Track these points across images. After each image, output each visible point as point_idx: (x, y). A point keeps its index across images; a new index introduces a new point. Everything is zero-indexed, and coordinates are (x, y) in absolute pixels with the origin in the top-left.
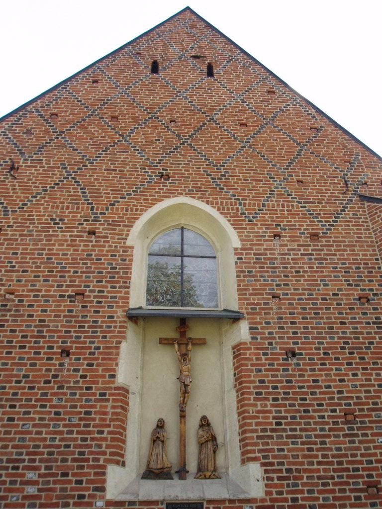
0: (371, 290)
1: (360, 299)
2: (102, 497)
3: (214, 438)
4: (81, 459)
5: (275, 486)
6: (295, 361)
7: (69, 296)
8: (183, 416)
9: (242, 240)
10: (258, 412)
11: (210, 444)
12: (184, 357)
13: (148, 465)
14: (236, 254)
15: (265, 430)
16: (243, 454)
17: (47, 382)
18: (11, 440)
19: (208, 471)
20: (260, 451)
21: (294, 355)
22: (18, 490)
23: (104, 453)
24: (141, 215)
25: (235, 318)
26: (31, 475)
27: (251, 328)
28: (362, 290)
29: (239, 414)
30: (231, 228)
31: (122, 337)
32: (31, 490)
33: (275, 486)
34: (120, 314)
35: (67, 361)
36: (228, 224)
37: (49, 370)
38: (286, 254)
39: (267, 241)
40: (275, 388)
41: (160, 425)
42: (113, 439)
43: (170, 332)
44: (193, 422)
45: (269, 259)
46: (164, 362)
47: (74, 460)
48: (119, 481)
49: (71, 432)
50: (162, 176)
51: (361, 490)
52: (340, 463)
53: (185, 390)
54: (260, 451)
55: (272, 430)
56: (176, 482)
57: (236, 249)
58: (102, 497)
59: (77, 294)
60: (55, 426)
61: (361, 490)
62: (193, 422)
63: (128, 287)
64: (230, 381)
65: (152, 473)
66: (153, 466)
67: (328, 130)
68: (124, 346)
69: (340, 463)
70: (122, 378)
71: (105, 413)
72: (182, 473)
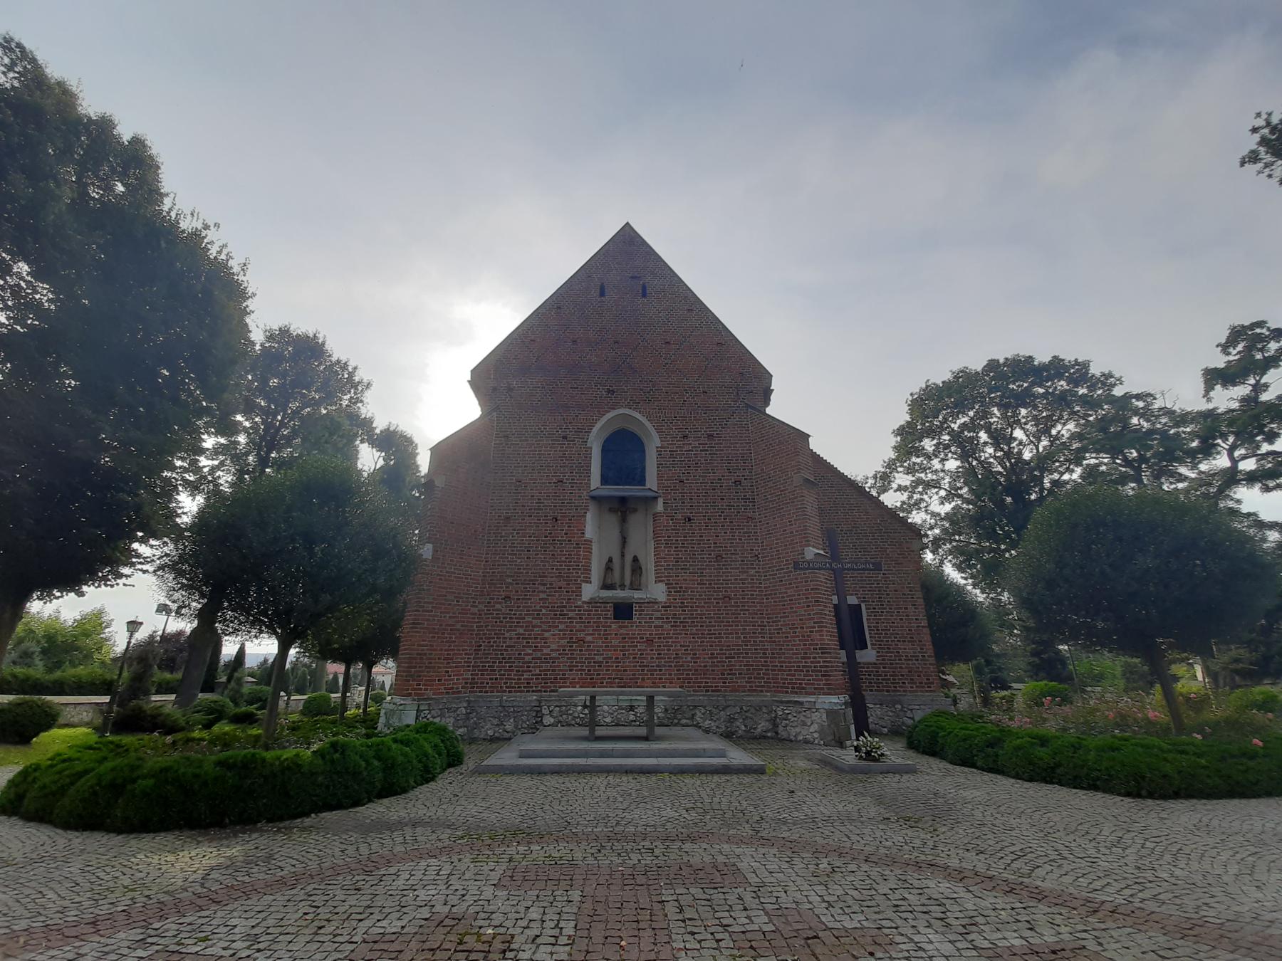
8: (623, 555)
12: (623, 520)
19: (635, 586)
41: (610, 560)
44: (629, 559)
50: (609, 391)
62: (629, 559)
65: (606, 586)
67: (238, 443)
68: (589, 515)
70: (588, 535)
72: (623, 587)
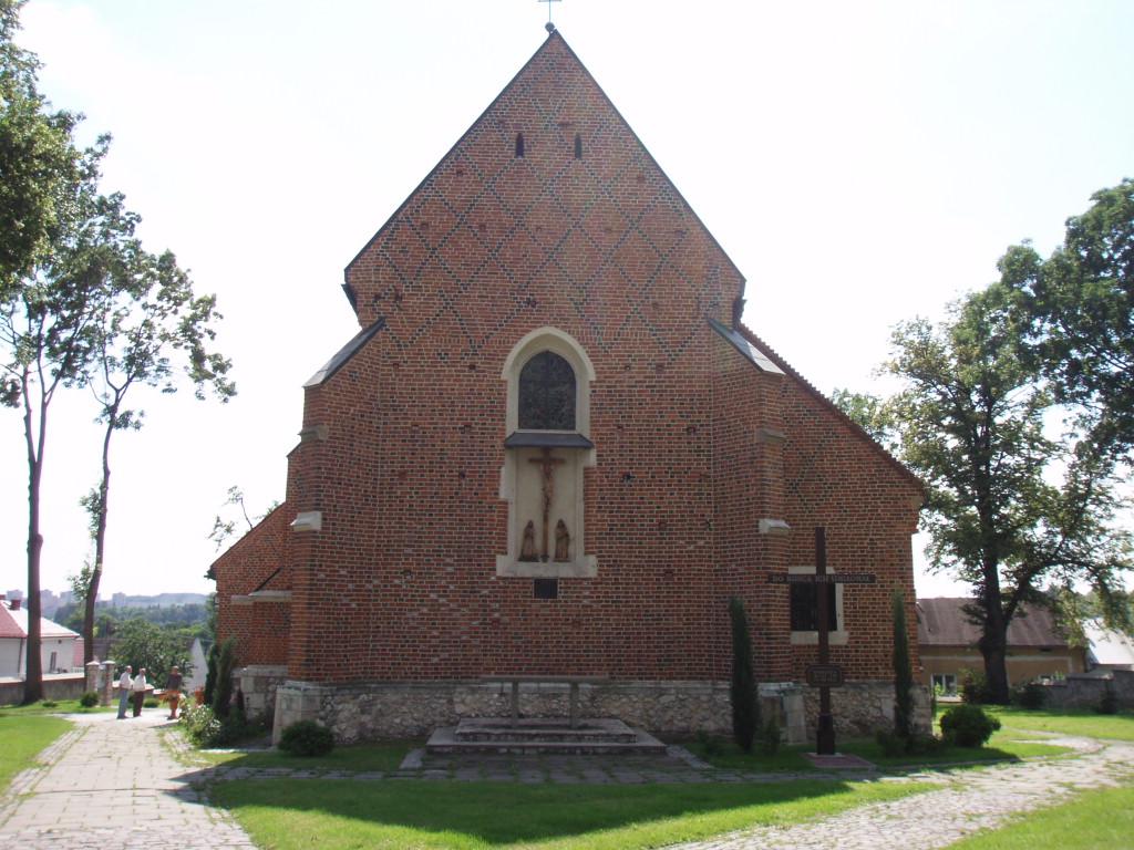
0: (699, 421)
1: (687, 430)
2: (494, 575)
3: (567, 535)
4: (479, 551)
5: (604, 570)
6: (629, 482)
7: (460, 428)
8: (546, 519)
9: (597, 373)
10: (598, 521)
11: (564, 540)
12: (547, 476)
13: (522, 551)
14: (592, 387)
15: (601, 534)
16: (586, 548)
17: (452, 498)
18: (434, 537)
19: (562, 557)
20: (596, 548)
21: (629, 477)
22: (443, 569)
23: (494, 547)
24: (511, 347)
25: (588, 447)
26: (448, 560)
27: (598, 456)
28: (692, 421)
29: (585, 521)
30: (588, 359)
31: (501, 463)
32: (450, 569)
33: (604, 570)
34: (499, 443)
35: (463, 482)
36: (586, 355)
37: (451, 489)
38: (633, 387)
39: (617, 373)
40: (612, 503)
42: (499, 538)
43: (538, 455)
44: (553, 524)
45: (619, 391)
46: (532, 481)
47: (475, 551)
48: (505, 565)
49: (471, 533)
51: (660, 575)
52: (668, 602)
53: (547, 502)
54: (596, 548)
55: (607, 534)
56: (541, 564)
57: (591, 382)
58: (494, 575)
59: (466, 426)
60: (460, 528)
61: (660, 575)
62: (553, 524)
63: (504, 420)
64: (581, 495)
66: (525, 553)
68: (503, 469)
69: (668, 602)
70: (502, 496)
71: (493, 520)
72: (545, 557)
